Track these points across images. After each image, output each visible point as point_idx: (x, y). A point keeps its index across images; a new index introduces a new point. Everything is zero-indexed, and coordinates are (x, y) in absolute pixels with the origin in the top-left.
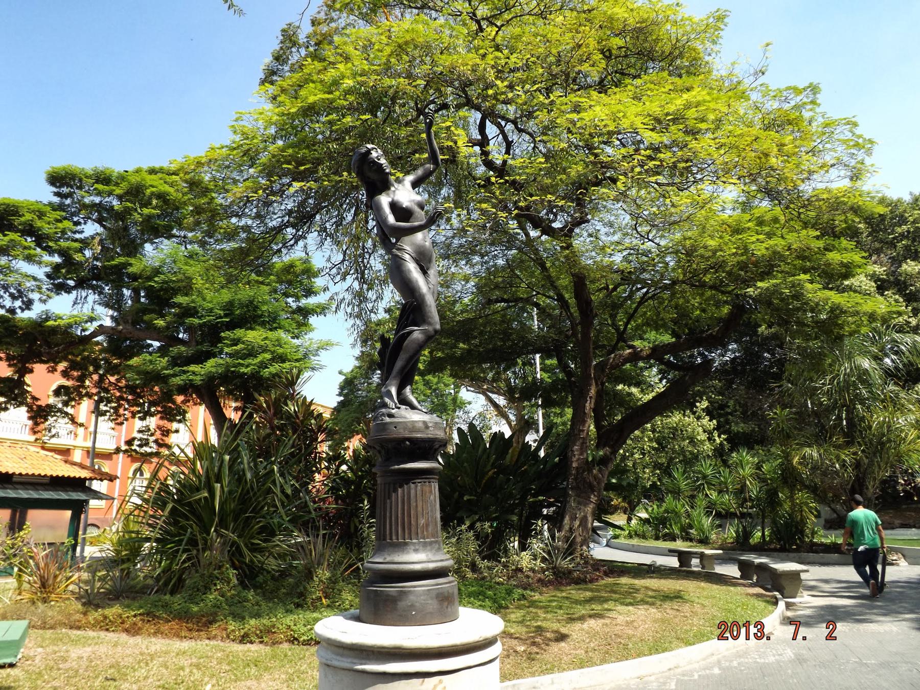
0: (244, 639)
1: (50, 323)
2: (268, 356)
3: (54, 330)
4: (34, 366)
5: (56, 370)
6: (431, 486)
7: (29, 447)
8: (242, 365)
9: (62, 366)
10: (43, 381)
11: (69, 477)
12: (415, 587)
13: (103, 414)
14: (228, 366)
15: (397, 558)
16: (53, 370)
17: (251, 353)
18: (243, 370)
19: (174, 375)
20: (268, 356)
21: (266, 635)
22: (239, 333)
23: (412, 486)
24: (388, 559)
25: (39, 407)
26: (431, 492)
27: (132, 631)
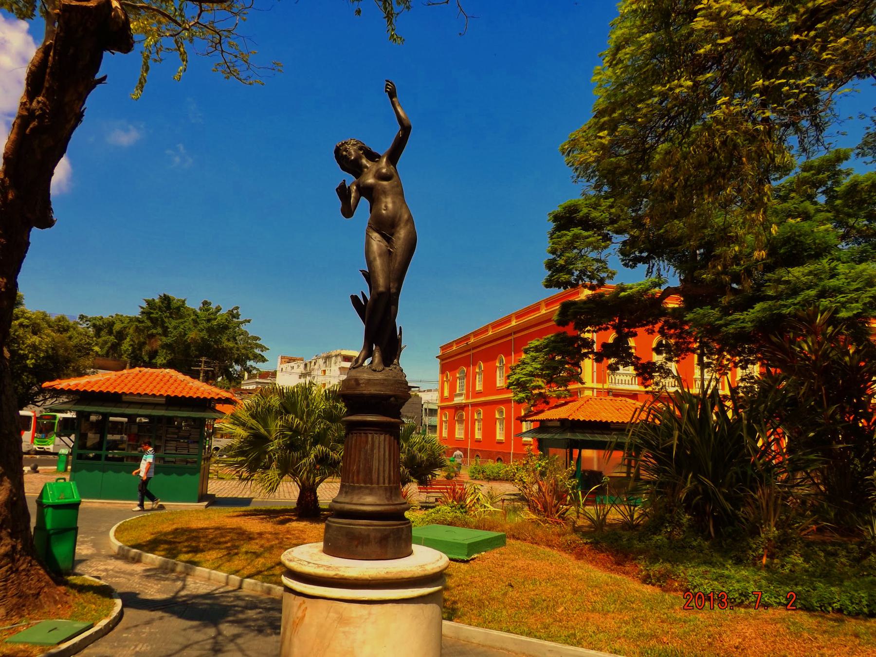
0: (646, 580)
1: (623, 294)
2: (812, 293)
3: (630, 298)
4: (637, 329)
5: (654, 331)
6: (367, 437)
7: (628, 399)
8: (785, 306)
9: (657, 327)
10: (644, 343)
11: (601, 421)
12: (334, 522)
13: (708, 365)
14: (770, 309)
15: (355, 499)
16: (651, 332)
17: (795, 291)
18: (785, 311)
19: (726, 325)
20: (812, 293)
21: (662, 581)
22: (782, 273)
23: (370, 436)
24: (362, 501)
25: (643, 364)
26: (367, 442)
27: (579, 556)
